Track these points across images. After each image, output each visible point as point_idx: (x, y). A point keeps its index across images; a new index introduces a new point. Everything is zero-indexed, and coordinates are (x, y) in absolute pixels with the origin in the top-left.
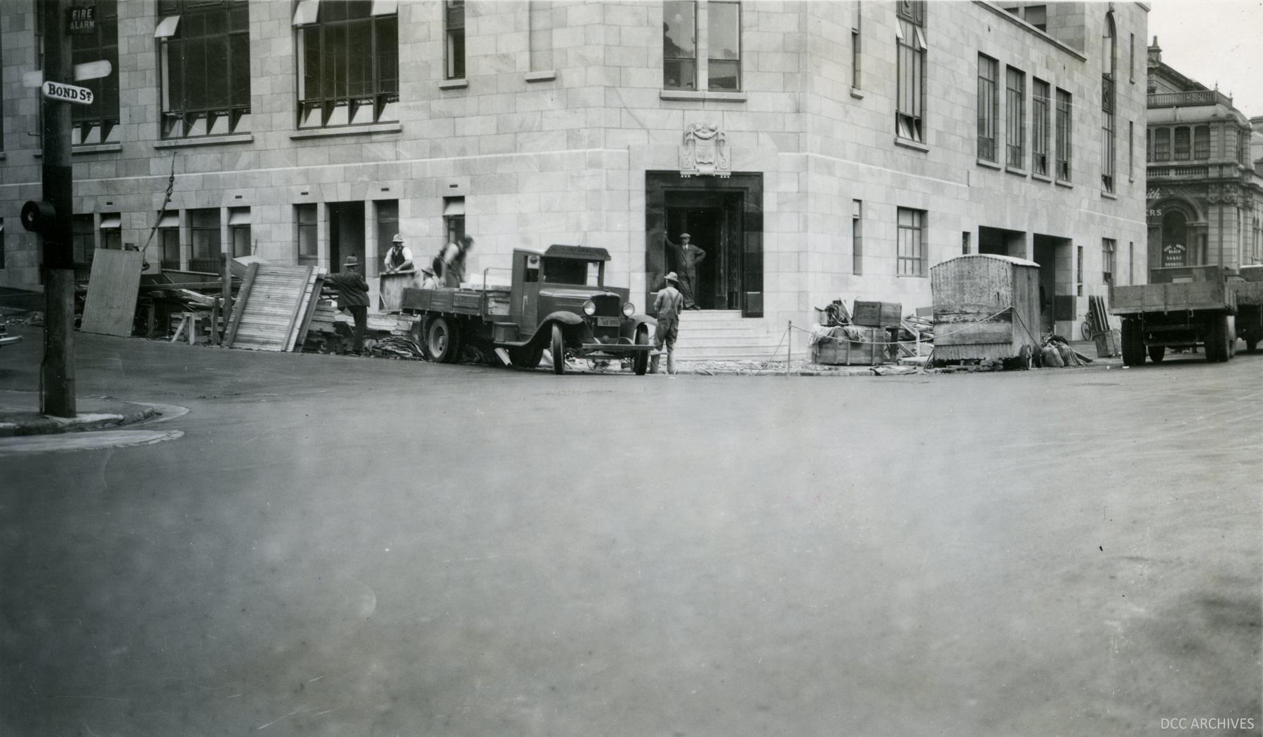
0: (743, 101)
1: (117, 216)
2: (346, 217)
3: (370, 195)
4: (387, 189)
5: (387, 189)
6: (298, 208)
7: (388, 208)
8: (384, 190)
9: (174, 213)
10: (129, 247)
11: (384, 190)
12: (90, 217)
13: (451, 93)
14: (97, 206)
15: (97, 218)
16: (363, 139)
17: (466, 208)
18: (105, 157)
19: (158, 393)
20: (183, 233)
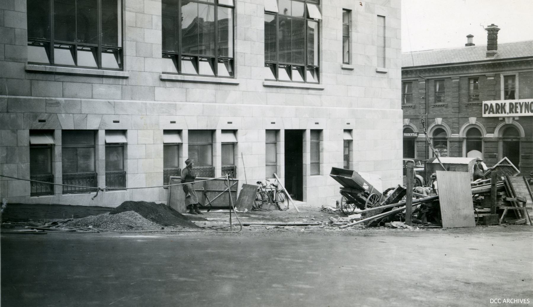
0: (237, 84)
1: (124, 132)
2: (294, 139)
3: (308, 126)
4: (317, 123)
5: (317, 123)
6: (268, 131)
7: (317, 133)
8: (172, 122)
9: (50, 133)
10: (347, 158)
11: (172, 122)
12: (95, 132)
13: (346, 71)
14: (102, 123)
15: (101, 133)
16: (305, 91)
17: (355, 137)
18: (111, 81)
19: (453, 267)
20: (58, 150)
